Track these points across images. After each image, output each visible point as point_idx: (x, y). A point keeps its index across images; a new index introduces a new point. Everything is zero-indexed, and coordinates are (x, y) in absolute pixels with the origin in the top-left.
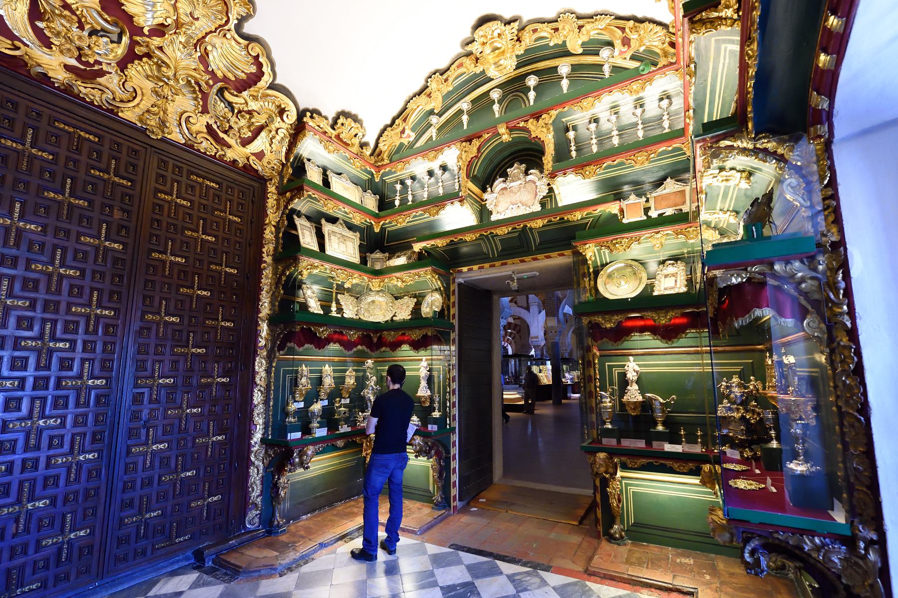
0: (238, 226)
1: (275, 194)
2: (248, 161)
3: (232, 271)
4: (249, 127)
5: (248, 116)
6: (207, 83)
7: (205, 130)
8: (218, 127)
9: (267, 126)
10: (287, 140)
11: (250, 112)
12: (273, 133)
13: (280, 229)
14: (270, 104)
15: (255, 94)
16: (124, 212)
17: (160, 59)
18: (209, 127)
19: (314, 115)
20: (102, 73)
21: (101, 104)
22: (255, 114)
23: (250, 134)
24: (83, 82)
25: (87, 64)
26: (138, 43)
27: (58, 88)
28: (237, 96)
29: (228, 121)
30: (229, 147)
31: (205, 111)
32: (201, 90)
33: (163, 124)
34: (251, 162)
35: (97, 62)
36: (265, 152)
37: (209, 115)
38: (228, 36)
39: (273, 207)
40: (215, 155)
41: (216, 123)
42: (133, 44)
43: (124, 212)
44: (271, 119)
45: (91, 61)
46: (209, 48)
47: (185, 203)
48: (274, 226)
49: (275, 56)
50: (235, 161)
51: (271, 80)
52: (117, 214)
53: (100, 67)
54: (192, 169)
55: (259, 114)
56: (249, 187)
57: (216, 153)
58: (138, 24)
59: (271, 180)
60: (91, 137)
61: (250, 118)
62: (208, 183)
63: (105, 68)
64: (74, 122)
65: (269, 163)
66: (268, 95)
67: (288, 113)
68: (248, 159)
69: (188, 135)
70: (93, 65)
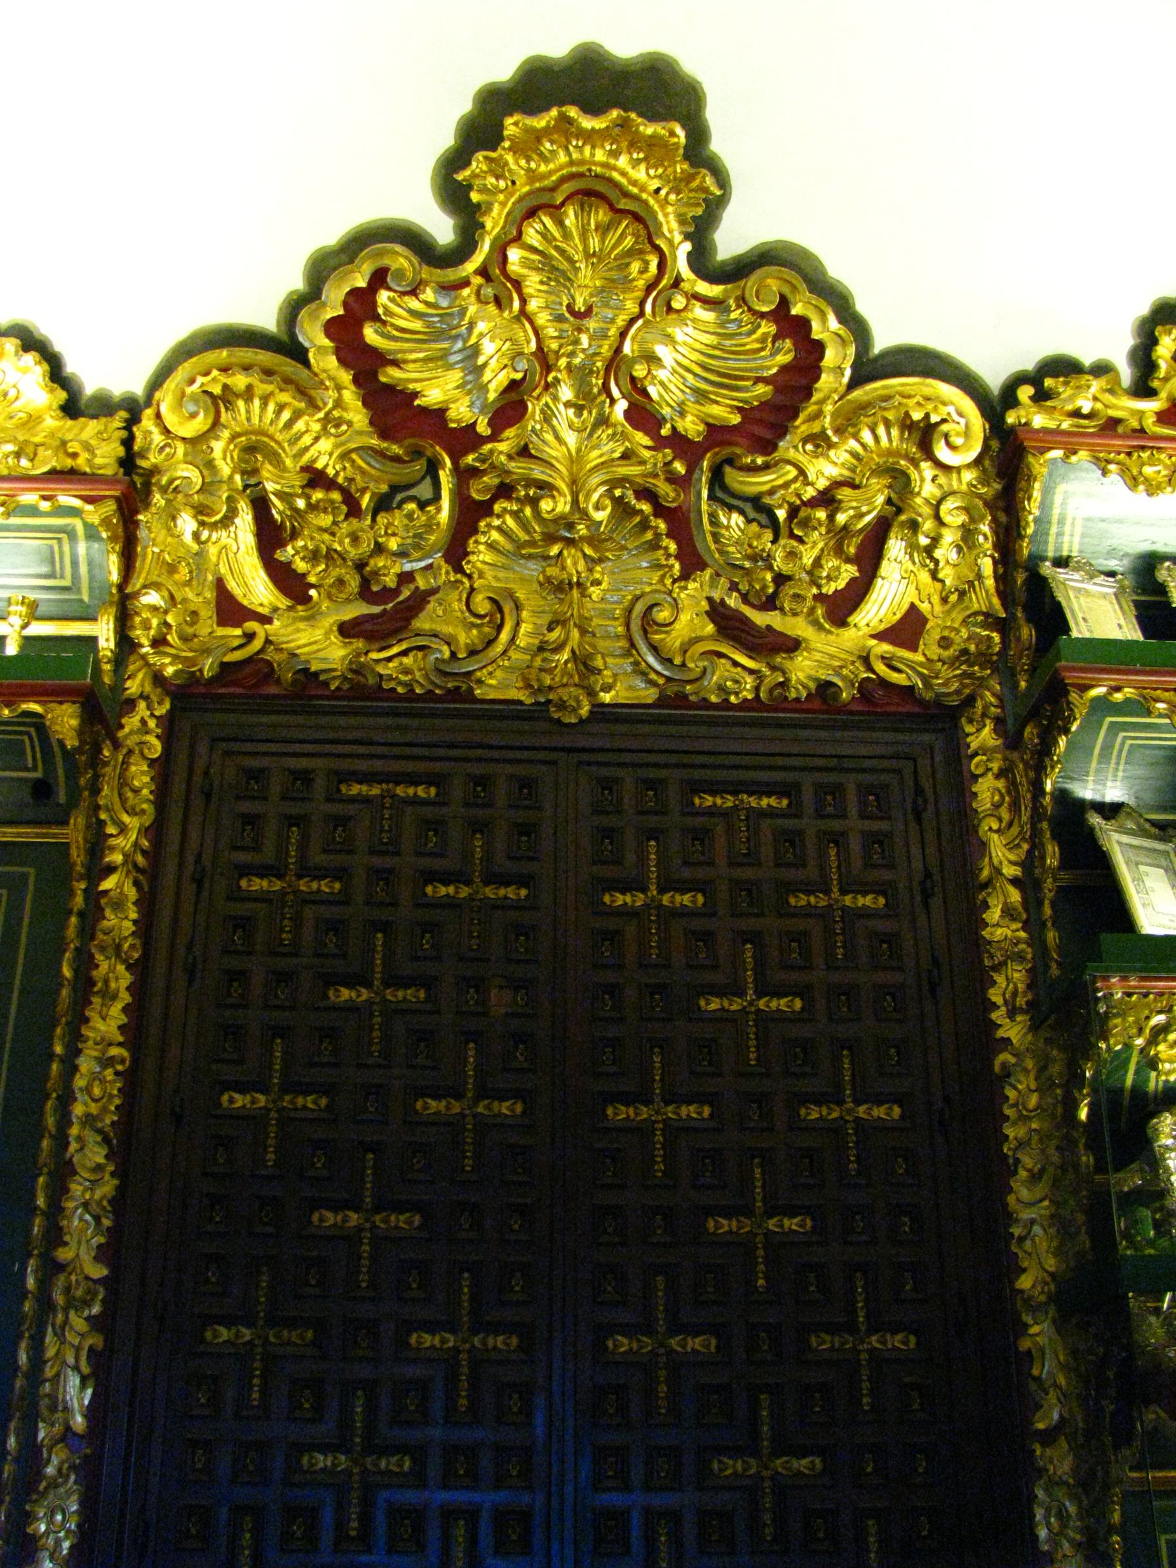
0: (880, 925)
1: (994, 750)
2: (870, 669)
3: (879, 1112)
4: (839, 551)
5: (821, 514)
6: (672, 478)
7: (710, 628)
8: (745, 598)
9: (899, 511)
10: (985, 528)
11: (827, 499)
12: (928, 525)
13: (1037, 885)
14: (881, 430)
15: (816, 428)
16: (517, 989)
17: (530, 482)
18: (717, 612)
19: (1048, 382)
20: (420, 600)
21: (430, 687)
22: (844, 493)
23: (849, 571)
24: (381, 650)
25: (388, 594)
26: (474, 472)
27: (337, 695)
28: (766, 467)
29: (768, 560)
30: (793, 645)
31: (692, 562)
32: (660, 510)
33: (584, 663)
34: (880, 668)
35: (406, 578)
36: (924, 607)
37: (708, 572)
38: (678, 302)
39: (997, 806)
40: (757, 696)
41: (734, 587)
42: (464, 475)
43: (517, 989)
44: (901, 484)
45: (390, 581)
46: (640, 371)
47: (686, 899)
48: (1015, 882)
49: (836, 269)
50: (825, 688)
51: (852, 350)
52: (499, 1000)
53: (412, 587)
54: (698, 774)
55: (855, 487)
56: (894, 764)
57: (757, 689)
58: (458, 421)
59: (970, 701)
60: (421, 791)
61: (831, 517)
62: (753, 802)
63: (421, 583)
64: (378, 765)
65: (945, 643)
66: (863, 408)
67: (944, 428)
68: (866, 660)
69: (658, 667)
70: (396, 592)
